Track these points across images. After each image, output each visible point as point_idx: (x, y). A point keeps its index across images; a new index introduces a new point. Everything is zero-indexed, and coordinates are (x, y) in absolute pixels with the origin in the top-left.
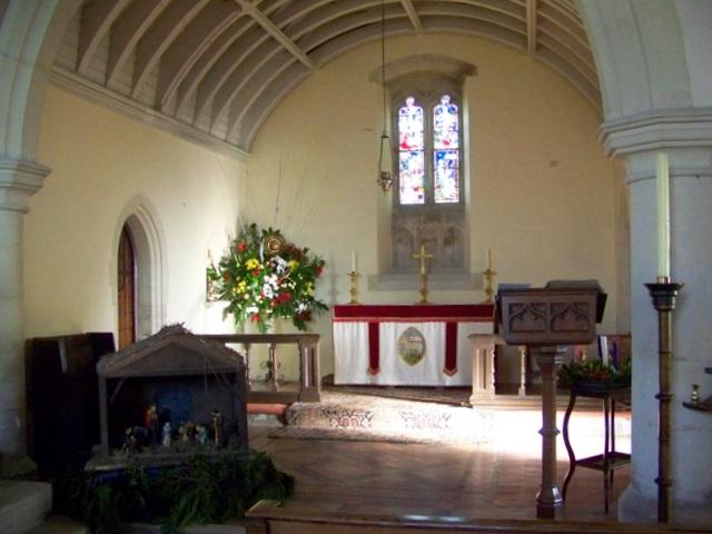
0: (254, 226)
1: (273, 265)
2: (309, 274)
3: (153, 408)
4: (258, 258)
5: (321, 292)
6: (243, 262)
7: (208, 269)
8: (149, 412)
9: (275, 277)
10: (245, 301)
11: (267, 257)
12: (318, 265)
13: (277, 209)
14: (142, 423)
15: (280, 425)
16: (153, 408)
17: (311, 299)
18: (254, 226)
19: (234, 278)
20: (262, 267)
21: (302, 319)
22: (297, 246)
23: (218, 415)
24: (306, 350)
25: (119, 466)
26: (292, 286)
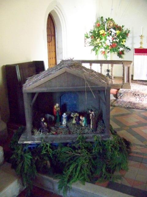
0: (102, 17)
1: (110, 32)
2: (124, 36)
3: (57, 105)
4: (104, 29)
5: (128, 43)
6: (99, 31)
7: (85, 34)
8: (55, 107)
9: (111, 37)
10: (99, 46)
11: (108, 30)
12: (127, 32)
13: (112, 9)
14: (52, 113)
15: (115, 98)
16: (57, 105)
17: (124, 46)
18: (102, 17)
19: (95, 37)
20: (106, 33)
21: (120, 54)
22: (119, 25)
23: (93, 113)
24: (126, 67)
25: (37, 142)
26: (118, 41)
